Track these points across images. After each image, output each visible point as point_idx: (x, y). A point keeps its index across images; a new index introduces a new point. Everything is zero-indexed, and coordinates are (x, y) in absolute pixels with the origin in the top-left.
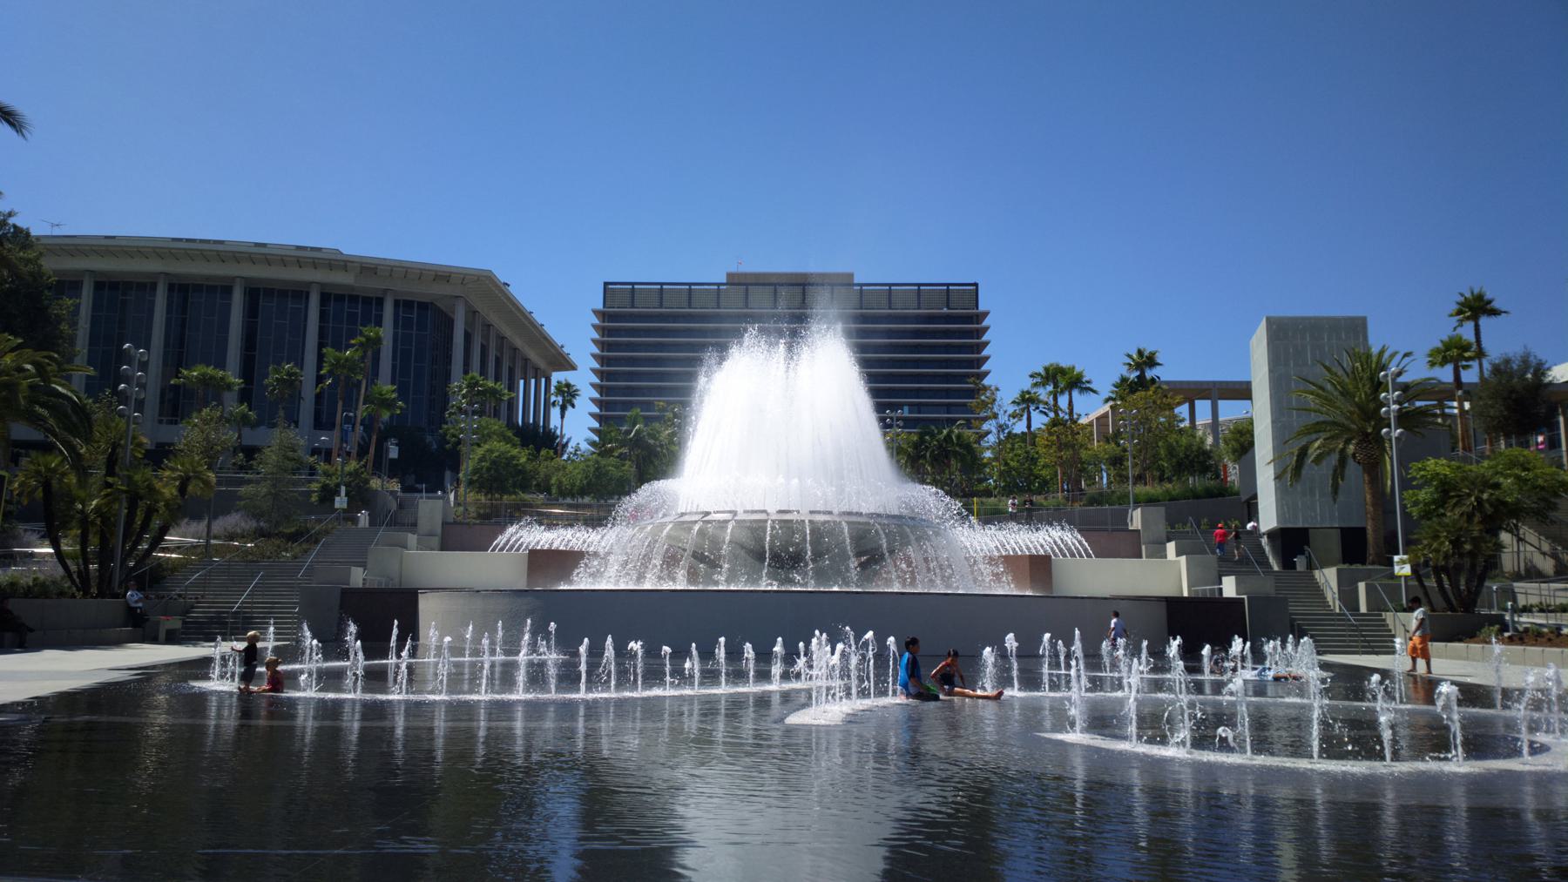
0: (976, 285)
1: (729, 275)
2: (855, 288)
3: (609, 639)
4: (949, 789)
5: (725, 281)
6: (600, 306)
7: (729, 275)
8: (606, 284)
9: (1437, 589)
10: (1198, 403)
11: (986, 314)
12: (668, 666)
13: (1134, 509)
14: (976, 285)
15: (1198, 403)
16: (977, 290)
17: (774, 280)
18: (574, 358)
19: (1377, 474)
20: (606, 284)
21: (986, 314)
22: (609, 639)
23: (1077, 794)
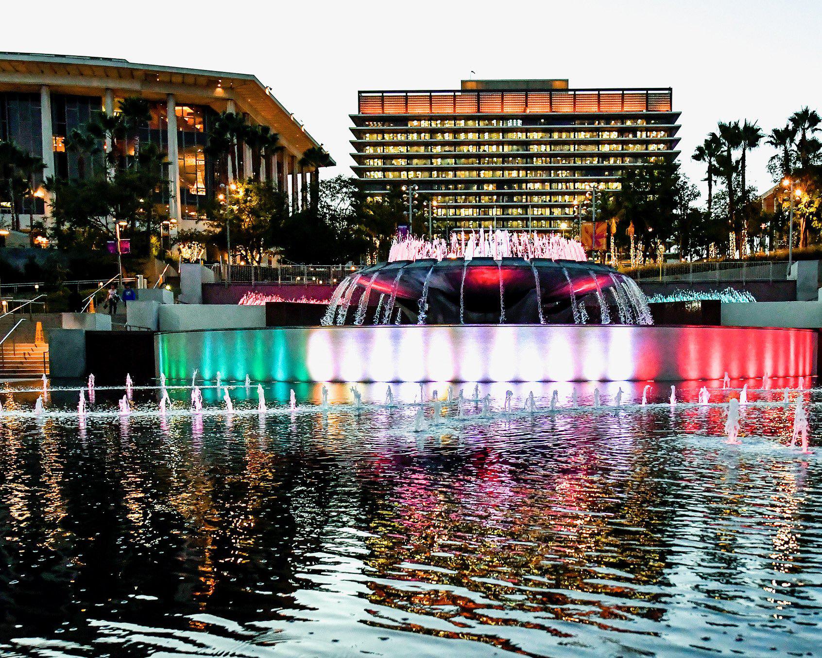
0: (670, 89)
1: (463, 82)
2: (570, 93)
3: (156, 598)
4: (690, 537)
5: (460, 89)
6: (355, 112)
7: (463, 82)
8: (360, 92)
9: (544, 134)
10: (521, 172)
11: (677, 115)
12: (284, 596)
13: (793, 263)
14: (670, 89)
15: (521, 172)
16: (671, 94)
17: (500, 87)
18: (334, 156)
19: (23, 62)
20: (360, 92)
21: (677, 115)
22: (156, 598)
23: (689, 257)
